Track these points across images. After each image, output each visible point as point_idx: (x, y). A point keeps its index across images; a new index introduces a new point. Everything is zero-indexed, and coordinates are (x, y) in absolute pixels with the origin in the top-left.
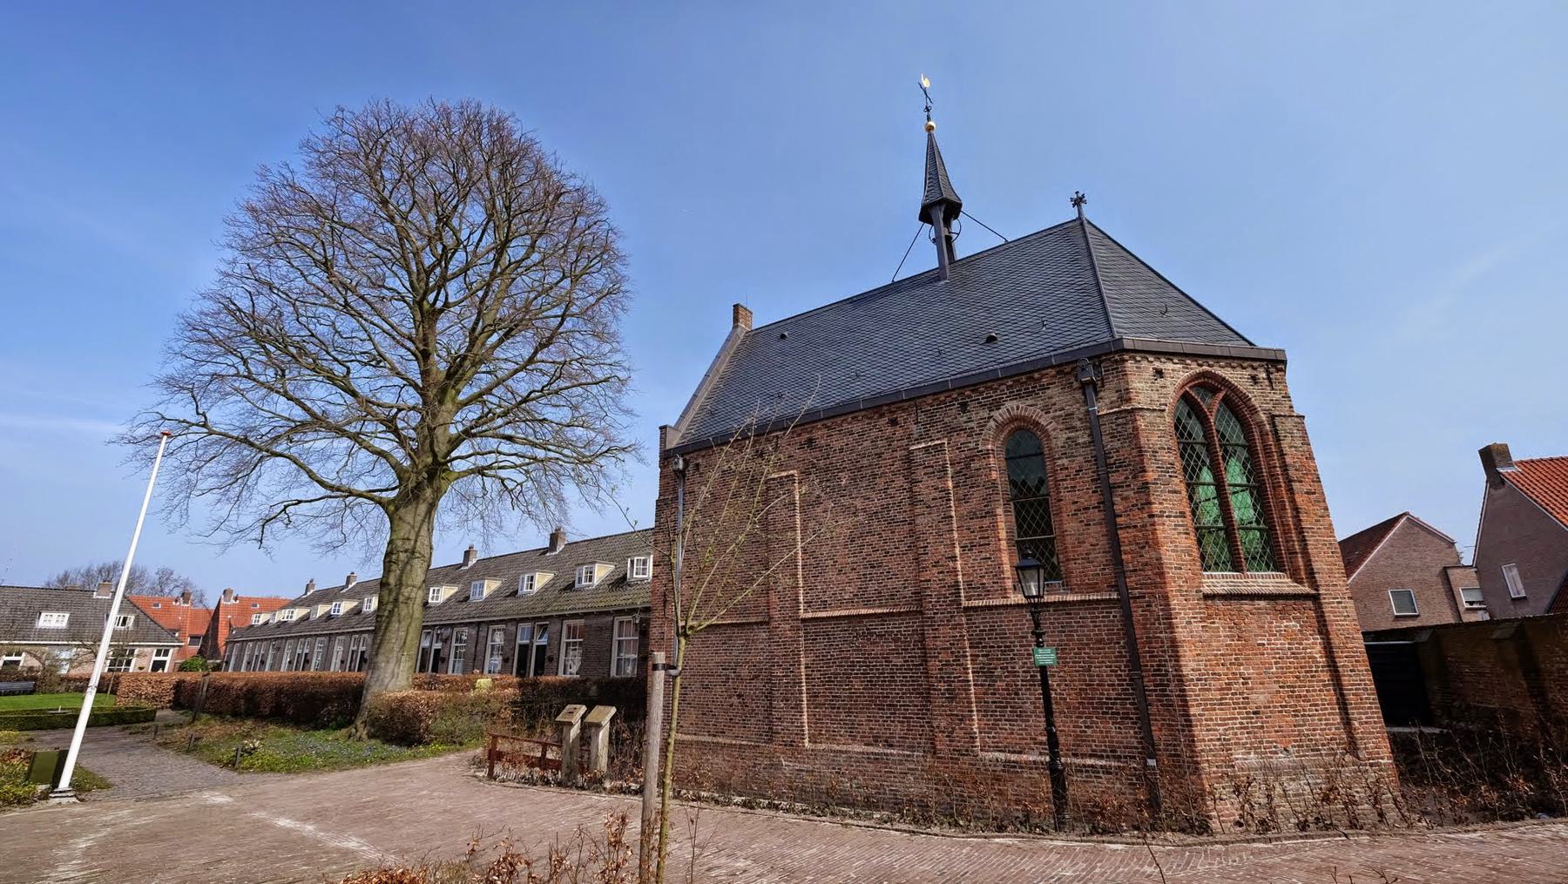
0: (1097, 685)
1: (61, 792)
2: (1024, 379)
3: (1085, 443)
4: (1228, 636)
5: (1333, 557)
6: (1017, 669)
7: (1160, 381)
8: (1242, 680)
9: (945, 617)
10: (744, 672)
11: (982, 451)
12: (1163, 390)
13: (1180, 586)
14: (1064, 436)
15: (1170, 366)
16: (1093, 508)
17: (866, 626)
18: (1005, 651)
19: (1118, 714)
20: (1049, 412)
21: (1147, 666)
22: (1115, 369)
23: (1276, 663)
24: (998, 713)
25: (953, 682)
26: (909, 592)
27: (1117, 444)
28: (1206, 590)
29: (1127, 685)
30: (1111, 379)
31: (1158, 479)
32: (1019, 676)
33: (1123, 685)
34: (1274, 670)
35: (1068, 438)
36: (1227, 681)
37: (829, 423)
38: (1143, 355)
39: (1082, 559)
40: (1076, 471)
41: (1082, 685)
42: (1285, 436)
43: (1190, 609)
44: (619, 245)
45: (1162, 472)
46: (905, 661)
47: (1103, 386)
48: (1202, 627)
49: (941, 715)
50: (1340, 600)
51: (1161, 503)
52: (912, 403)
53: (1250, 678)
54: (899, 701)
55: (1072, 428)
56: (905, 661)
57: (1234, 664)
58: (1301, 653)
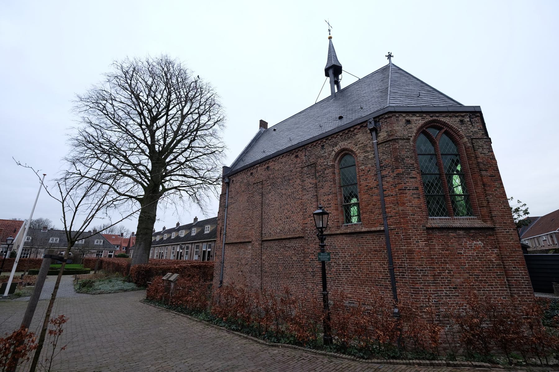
0: (374, 271)
1: (5, 297)
2: (347, 132)
3: (372, 158)
4: (440, 249)
5: (505, 208)
6: (340, 263)
7: (409, 126)
8: (447, 271)
9: (312, 239)
10: (243, 262)
11: (329, 165)
12: (410, 129)
13: (413, 224)
14: (363, 155)
15: (415, 118)
16: (374, 188)
17: (284, 243)
18: (336, 255)
19: (383, 286)
20: (357, 145)
21: (396, 263)
22: (386, 122)
23: (468, 263)
24: (332, 283)
25: (315, 268)
26: (300, 229)
27: (385, 157)
28: (429, 225)
29: (387, 272)
30: (384, 126)
31: (404, 172)
32: (341, 266)
33: (385, 272)
34: (467, 266)
35: (365, 156)
36: (438, 271)
37: (274, 159)
38: (400, 114)
39: (369, 212)
40: (368, 171)
41: (367, 271)
42: (479, 148)
43: (418, 235)
44: (218, 100)
45: (406, 168)
46: (297, 259)
48: (425, 244)
49: (309, 283)
50: (508, 231)
51: (404, 183)
52: (304, 147)
53: (452, 270)
54: (295, 276)
55: (367, 152)
56: (297, 259)
57: (443, 263)
58: (484, 258)
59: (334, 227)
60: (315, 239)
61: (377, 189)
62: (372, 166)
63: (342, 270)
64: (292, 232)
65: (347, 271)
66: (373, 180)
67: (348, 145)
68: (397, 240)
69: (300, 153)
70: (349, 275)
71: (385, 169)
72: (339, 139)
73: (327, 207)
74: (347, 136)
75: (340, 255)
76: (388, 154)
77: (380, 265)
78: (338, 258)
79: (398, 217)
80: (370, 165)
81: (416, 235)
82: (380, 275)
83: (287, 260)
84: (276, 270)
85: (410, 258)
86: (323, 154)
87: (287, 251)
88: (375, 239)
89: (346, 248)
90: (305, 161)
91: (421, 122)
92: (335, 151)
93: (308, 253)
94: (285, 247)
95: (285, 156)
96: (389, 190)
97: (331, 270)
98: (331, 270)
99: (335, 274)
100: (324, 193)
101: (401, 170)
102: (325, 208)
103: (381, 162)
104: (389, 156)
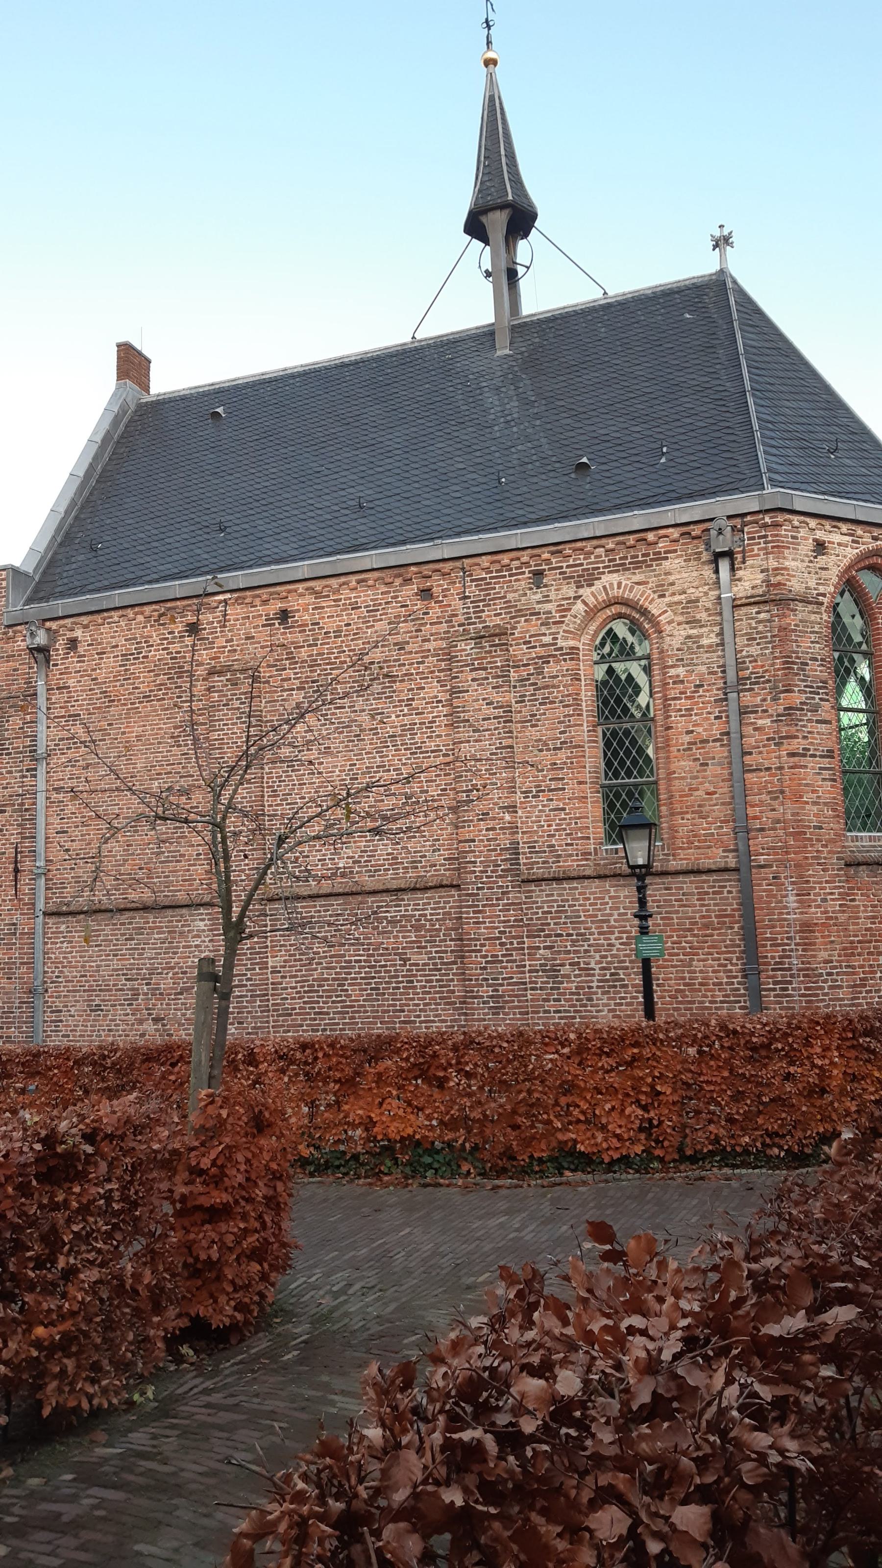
0: (701, 984)
3: (710, 646)
6: (592, 965)
7: (822, 560)
11: (561, 649)
12: (824, 572)
15: (836, 538)
16: (714, 741)
18: (578, 941)
20: (663, 596)
21: (766, 957)
25: (502, 985)
29: (739, 983)
30: (756, 552)
32: (593, 975)
33: (733, 983)
35: (689, 637)
39: (693, 812)
41: (679, 985)
43: (827, 882)
45: (811, 692)
46: (429, 959)
47: (744, 562)
48: (840, 905)
51: (805, 737)
54: (419, 1016)
56: (429, 959)
59: (571, 855)
60: (508, 893)
61: (722, 746)
62: (709, 673)
63: (598, 987)
64: (406, 868)
65: (615, 986)
66: (712, 717)
67: (632, 588)
68: (775, 896)
69: (438, 585)
70: (622, 998)
71: (753, 689)
72: (603, 562)
73: (550, 790)
74: (632, 557)
75: (592, 942)
76: (766, 643)
77: (719, 965)
78: (586, 951)
79: (781, 832)
80: (703, 669)
81: (821, 883)
82: (717, 993)
83: (385, 966)
84: (333, 1002)
85: (805, 944)
86: (538, 603)
87: (385, 932)
88: (707, 893)
89: (615, 921)
90: (461, 618)
91: (851, 553)
92: (584, 602)
93: (479, 940)
94: (377, 919)
95: (370, 582)
96: (760, 753)
97: (559, 988)
98: (559, 988)
99: (571, 1000)
100: (540, 740)
101: (797, 698)
102: (543, 791)
103: (740, 665)
104: (767, 648)
